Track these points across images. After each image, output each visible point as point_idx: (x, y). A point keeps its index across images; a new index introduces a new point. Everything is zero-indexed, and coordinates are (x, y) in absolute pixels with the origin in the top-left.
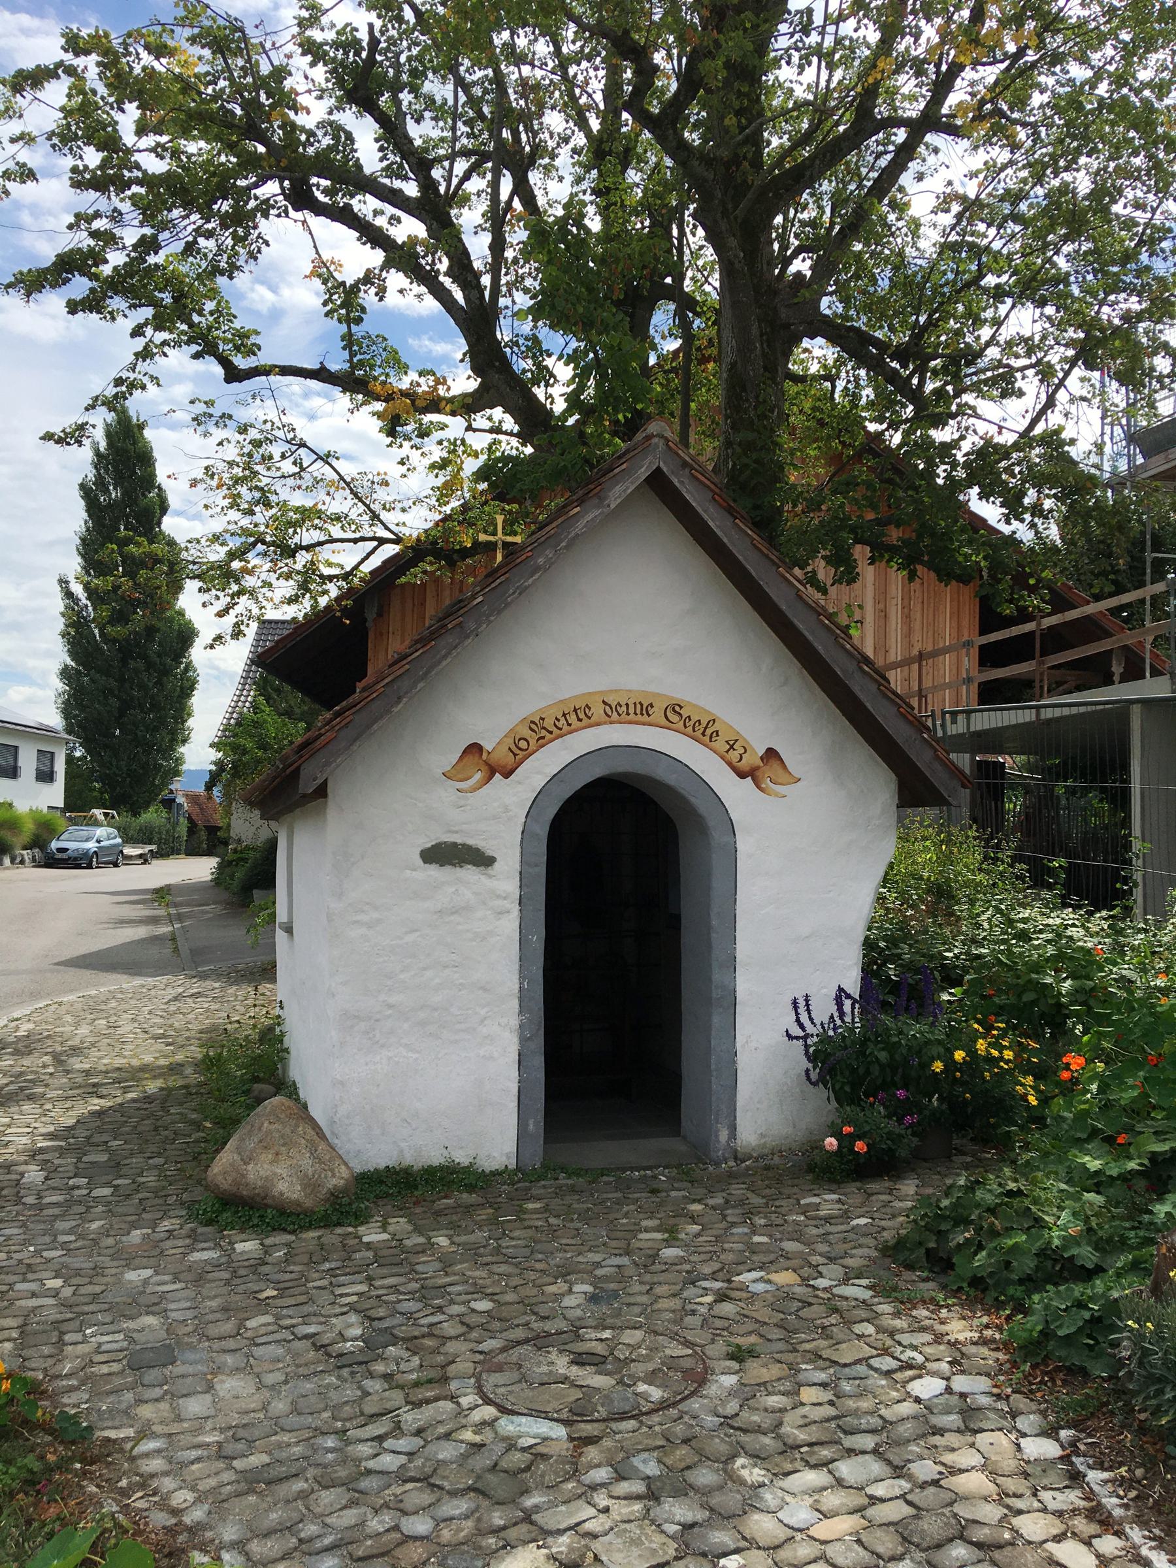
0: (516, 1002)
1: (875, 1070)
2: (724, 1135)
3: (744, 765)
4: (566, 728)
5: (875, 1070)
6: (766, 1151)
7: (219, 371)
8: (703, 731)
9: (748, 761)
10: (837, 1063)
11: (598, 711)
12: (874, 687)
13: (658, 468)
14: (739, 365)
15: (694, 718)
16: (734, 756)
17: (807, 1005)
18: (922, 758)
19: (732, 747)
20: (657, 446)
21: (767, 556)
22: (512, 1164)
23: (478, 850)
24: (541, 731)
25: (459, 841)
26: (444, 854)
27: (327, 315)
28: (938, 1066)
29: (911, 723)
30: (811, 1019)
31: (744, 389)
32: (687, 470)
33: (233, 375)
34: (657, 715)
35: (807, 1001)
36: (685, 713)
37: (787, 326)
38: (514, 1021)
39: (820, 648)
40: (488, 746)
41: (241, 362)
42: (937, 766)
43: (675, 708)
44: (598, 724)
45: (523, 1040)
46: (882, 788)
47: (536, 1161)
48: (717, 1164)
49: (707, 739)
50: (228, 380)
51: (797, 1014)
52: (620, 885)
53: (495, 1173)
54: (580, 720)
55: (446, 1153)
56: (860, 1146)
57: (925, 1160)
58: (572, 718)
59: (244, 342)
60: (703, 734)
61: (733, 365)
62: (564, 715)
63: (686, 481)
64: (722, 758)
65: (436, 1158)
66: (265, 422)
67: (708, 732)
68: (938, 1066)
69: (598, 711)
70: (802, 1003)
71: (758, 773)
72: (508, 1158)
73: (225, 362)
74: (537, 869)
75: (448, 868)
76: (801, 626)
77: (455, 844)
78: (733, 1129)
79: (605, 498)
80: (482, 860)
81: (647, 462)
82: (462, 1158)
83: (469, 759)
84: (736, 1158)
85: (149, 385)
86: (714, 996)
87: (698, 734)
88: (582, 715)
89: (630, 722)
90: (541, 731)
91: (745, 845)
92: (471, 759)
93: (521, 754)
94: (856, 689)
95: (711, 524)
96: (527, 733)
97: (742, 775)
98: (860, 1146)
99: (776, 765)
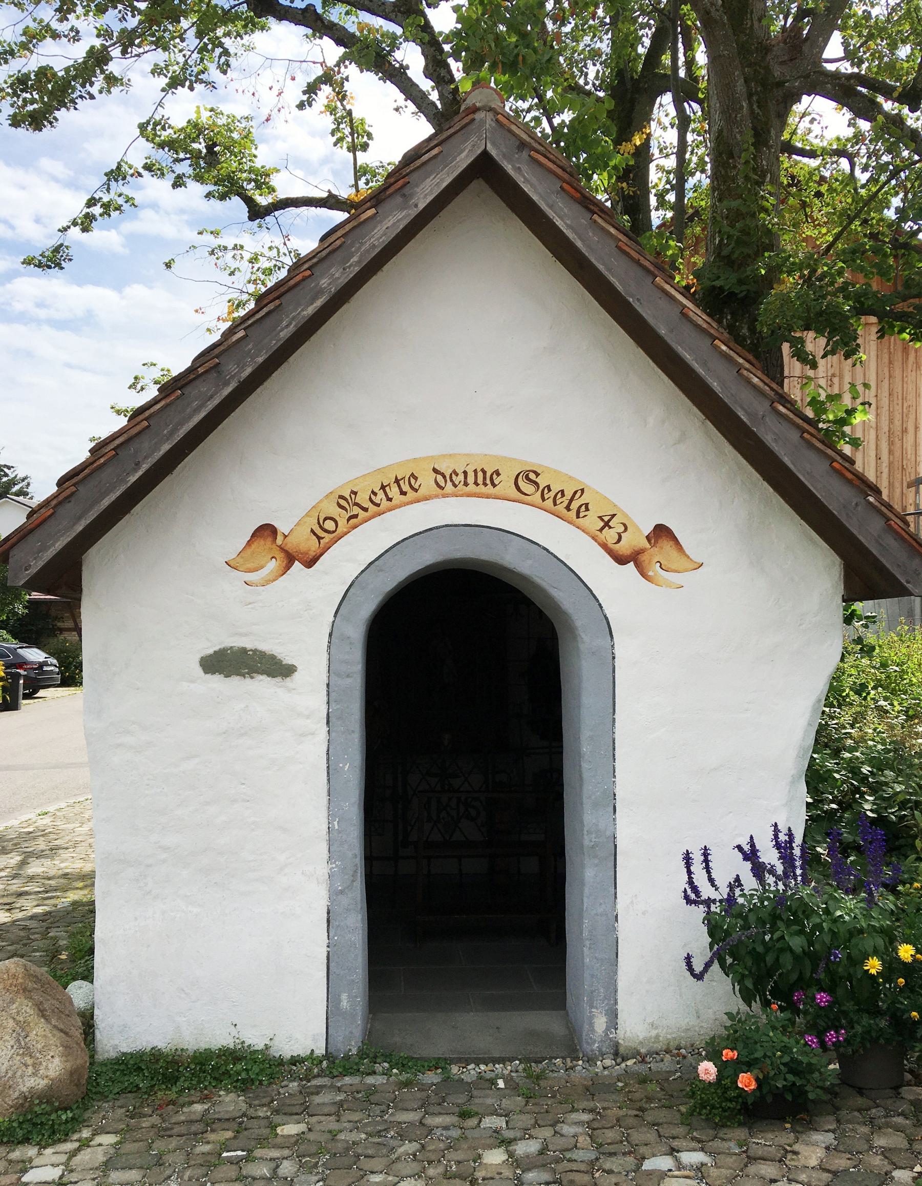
0: (324, 847)
1: (787, 961)
2: (600, 1023)
3: (624, 547)
4: (385, 504)
5: (787, 961)
6: (657, 1046)
7: (244, 209)
8: (569, 504)
9: (632, 541)
10: (751, 942)
11: (427, 481)
12: (794, 435)
13: (485, 154)
14: (725, 131)
15: (555, 488)
16: (610, 536)
17: (706, 861)
18: (868, 532)
19: (607, 524)
20: (483, 122)
21: (638, 262)
22: (320, 1051)
23: (273, 657)
24: (353, 508)
25: (249, 646)
26: (226, 663)
27: (335, 144)
28: (874, 965)
29: (850, 482)
30: (711, 880)
31: (731, 155)
32: (525, 154)
33: (256, 213)
34: (506, 484)
35: (706, 854)
36: (542, 481)
37: (780, 84)
38: (322, 869)
39: (715, 385)
40: (283, 527)
41: (263, 200)
42: (890, 541)
43: (529, 476)
44: (426, 498)
45: (334, 894)
46: (818, 574)
47: (351, 1040)
48: (591, 1060)
49: (573, 514)
50: (251, 218)
51: (689, 873)
52: (466, 702)
53: (295, 1061)
54: (403, 493)
55: (234, 1032)
56: (746, 1081)
57: (860, 1091)
58: (394, 492)
59: (262, 179)
60: (568, 508)
61: (720, 132)
62: (383, 488)
63: (524, 168)
64: (594, 538)
65: (218, 1037)
66: (270, 248)
67: (575, 505)
68: (874, 965)
69: (427, 481)
70: (697, 858)
71: (644, 558)
72: (315, 1039)
73: (249, 201)
74: (349, 681)
75: (235, 680)
76: (687, 357)
77: (244, 651)
78: (613, 1016)
79: (412, 196)
80: (278, 669)
81: (468, 145)
82: (255, 1039)
83: (259, 544)
84: (616, 1054)
85: (126, 207)
86: (586, 842)
87: (561, 508)
88: (406, 488)
89: (469, 495)
90: (353, 508)
91: (626, 649)
92: (262, 545)
93: (327, 537)
94: (768, 439)
95: (559, 223)
96: (335, 511)
97: (621, 560)
98: (746, 1081)
99: (666, 545)
